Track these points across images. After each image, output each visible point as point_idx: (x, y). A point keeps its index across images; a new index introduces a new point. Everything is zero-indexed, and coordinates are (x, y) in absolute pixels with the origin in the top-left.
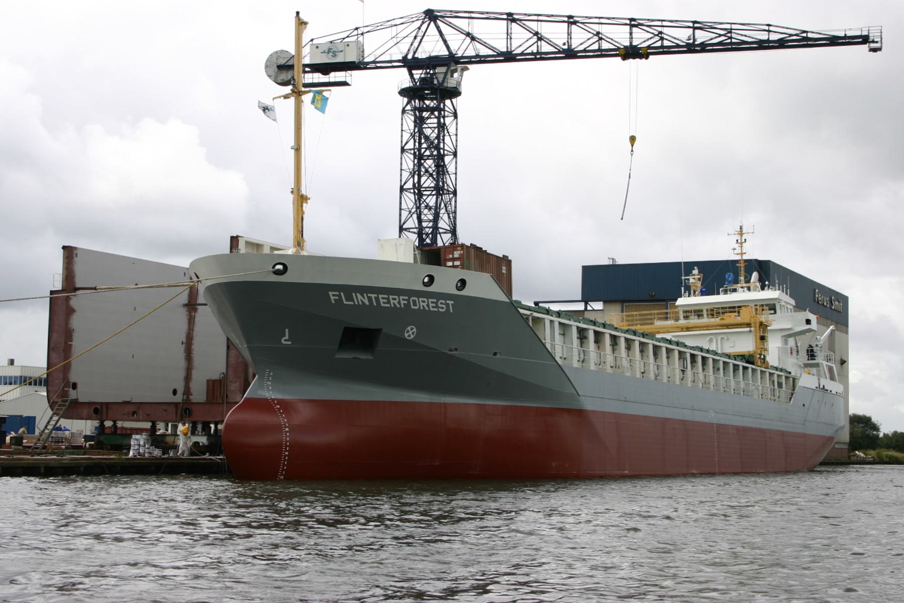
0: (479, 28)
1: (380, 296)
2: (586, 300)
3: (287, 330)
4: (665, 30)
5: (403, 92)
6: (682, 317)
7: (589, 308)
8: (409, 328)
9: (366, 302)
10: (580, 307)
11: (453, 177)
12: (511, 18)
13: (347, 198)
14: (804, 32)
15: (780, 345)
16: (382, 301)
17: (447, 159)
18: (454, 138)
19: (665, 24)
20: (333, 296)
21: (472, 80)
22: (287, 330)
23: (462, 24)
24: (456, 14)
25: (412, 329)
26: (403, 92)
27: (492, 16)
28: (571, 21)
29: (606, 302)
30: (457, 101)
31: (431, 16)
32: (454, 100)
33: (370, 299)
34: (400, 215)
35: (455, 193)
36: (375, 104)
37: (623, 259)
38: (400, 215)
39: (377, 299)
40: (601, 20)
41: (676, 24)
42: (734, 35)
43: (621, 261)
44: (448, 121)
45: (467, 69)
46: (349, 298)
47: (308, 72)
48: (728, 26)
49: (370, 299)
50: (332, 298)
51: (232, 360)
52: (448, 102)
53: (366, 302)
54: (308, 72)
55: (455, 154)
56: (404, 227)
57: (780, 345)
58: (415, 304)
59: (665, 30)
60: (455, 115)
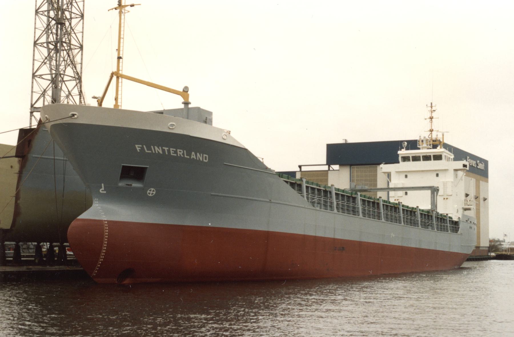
1: (171, 149)
2: (329, 163)
3: (103, 185)
6: (307, 185)
7: (331, 169)
8: (150, 195)
9: (161, 152)
10: (326, 168)
15: (452, 180)
16: (172, 152)
22: (103, 185)
25: (149, 193)
29: (341, 165)
33: (163, 151)
34: (33, 64)
37: (353, 139)
38: (33, 64)
39: (169, 151)
43: (350, 141)
46: (149, 148)
49: (163, 151)
50: (138, 149)
53: (161, 152)
56: (36, 74)
57: (452, 180)
58: (206, 157)
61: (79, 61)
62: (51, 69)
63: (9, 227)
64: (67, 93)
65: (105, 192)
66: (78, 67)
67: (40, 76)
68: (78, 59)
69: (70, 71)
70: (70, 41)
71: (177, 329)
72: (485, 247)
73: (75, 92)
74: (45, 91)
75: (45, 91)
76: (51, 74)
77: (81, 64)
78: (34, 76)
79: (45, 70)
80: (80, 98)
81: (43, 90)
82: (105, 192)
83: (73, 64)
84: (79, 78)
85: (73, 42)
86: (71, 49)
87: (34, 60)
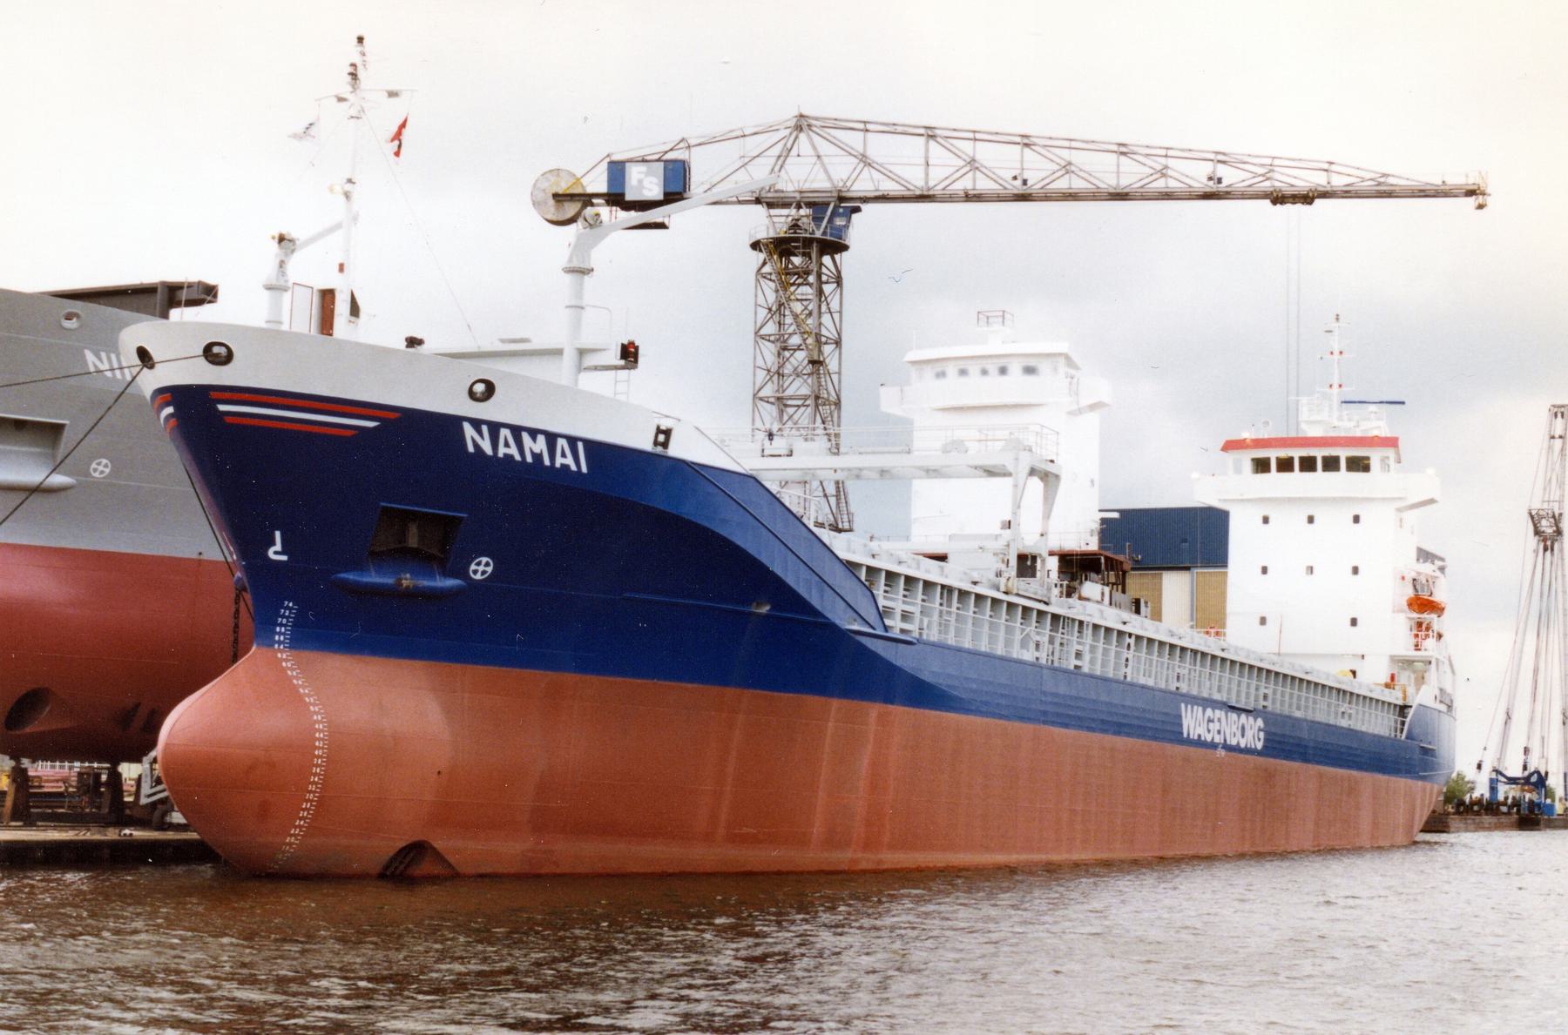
0: (879, 147)
4: (1171, 163)
5: (845, 248)
11: (835, 377)
12: (930, 134)
13: (649, 363)
14: (1384, 175)
17: (827, 349)
18: (836, 316)
19: (1074, 144)
20: (469, 430)
21: (862, 229)
23: (854, 139)
24: (838, 124)
26: (845, 248)
27: (900, 129)
28: (1026, 142)
30: (844, 258)
31: (802, 124)
32: (837, 257)
35: (838, 404)
36: (715, 243)
40: (1071, 143)
41: (1189, 155)
42: (1276, 176)
44: (827, 289)
45: (857, 210)
47: (632, 195)
48: (1268, 161)
51: (213, 394)
52: (827, 260)
54: (632, 195)
55: (838, 343)
59: (1171, 163)
60: (839, 281)
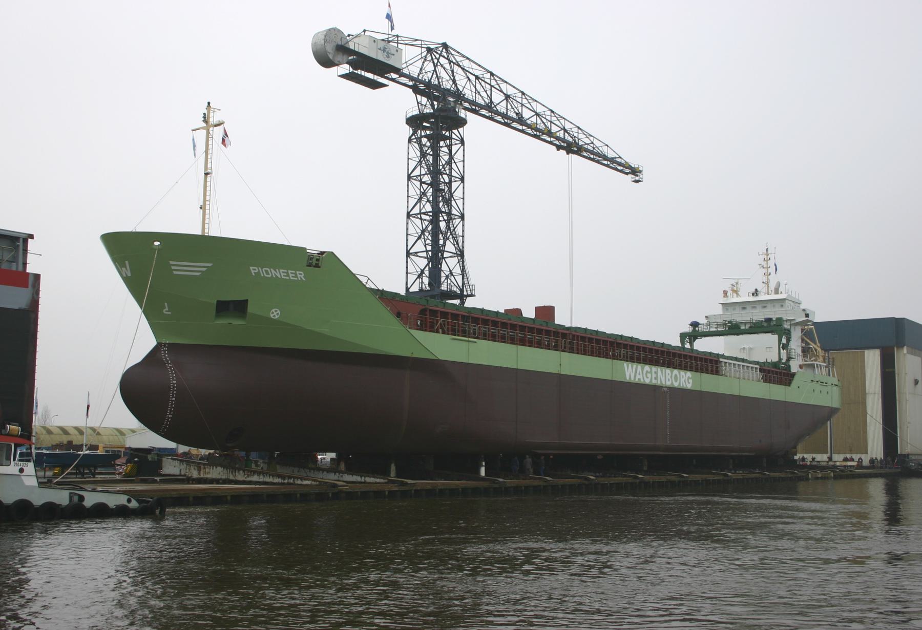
61: (461, 234)
62: (425, 245)
63: (155, 343)
64: (447, 273)
65: (171, 262)
66: (460, 239)
67: (416, 254)
68: (459, 231)
69: (450, 247)
70: (450, 211)
71: (859, 523)
72: (25, 264)
73: (457, 270)
74: (422, 271)
75: (422, 271)
76: (427, 251)
77: (463, 236)
78: (408, 254)
79: (419, 247)
80: (463, 278)
81: (419, 271)
82: (171, 262)
83: (455, 238)
84: (460, 254)
85: (454, 212)
86: (451, 219)
87: (407, 235)
